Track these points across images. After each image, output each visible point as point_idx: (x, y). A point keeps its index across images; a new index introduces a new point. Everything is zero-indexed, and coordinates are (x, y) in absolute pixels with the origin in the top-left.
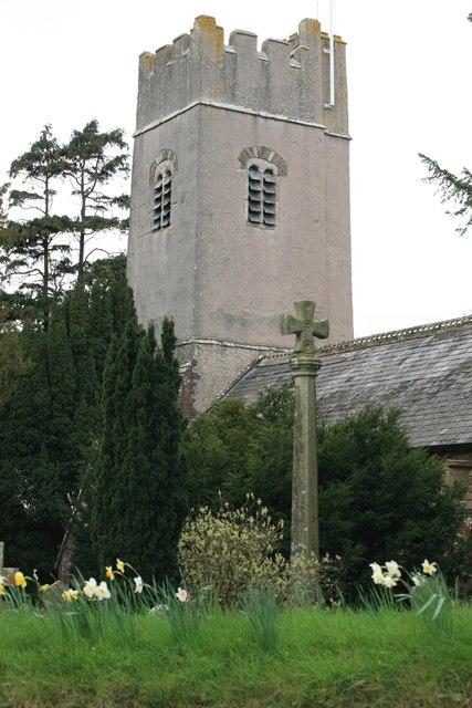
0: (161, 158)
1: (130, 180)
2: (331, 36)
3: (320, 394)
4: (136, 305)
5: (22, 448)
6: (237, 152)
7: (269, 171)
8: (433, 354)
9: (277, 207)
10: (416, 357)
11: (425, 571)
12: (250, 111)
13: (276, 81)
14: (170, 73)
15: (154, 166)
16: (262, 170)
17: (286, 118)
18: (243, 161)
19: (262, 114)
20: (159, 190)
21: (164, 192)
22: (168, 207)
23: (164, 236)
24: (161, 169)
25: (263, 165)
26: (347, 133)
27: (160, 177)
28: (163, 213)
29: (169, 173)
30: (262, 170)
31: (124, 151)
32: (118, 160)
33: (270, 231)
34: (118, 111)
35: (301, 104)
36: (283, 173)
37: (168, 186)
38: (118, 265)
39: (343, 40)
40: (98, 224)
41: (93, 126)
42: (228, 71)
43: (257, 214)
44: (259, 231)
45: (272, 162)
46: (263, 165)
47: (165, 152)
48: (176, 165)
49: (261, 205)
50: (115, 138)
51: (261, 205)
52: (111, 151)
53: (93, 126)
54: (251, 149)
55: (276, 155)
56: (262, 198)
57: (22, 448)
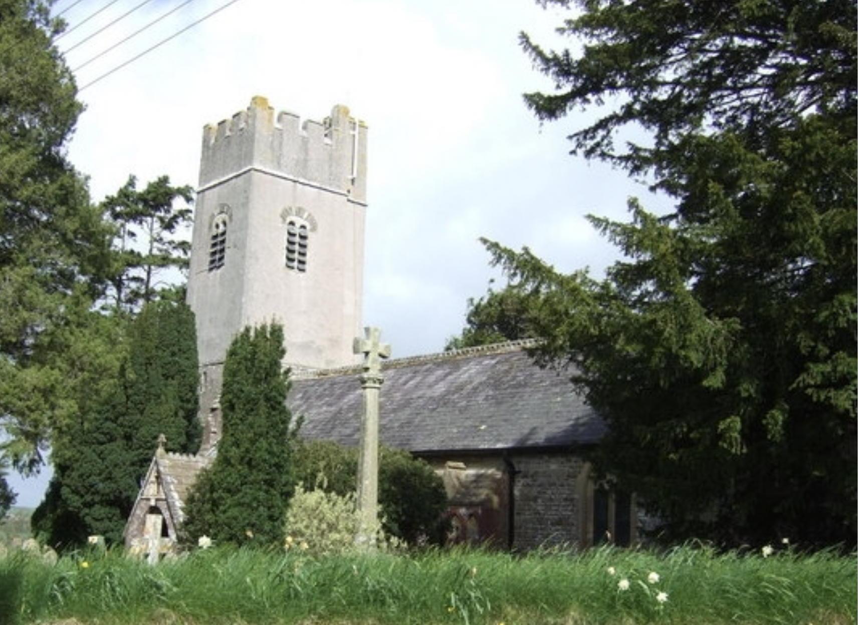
0: (218, 211)
1: (191, 229)
2: (357, 121)
3: (567, 88)
4: (197, 327)
5: (102, 438)
6: (280, 211)
7: (303, 227)
8: (432, 378)
9: (309, 247)
10: (418, 379)
11: (97, 506)
12: (291, 177)
13: (312, 155)
14: (229, 143)
15: (213, 217)
16: (298, 225)
17: (318, 185)
18: (284, 217)
19: (302, 180)
20: (215, 237)
21: (220, 239)
22: (222, 250)
23: (218, 276)
24: (219, 219)
25: (299, 222)
26: (365, 200)
27: (217, 226)
28: (217, 256)
29: (225, 223)
30: (298, 225)
31: (191, 207)
32: (183, 213)
33: (301, 275)
34: (184, 172)
35: (331, 174)
36: (314, 229)
37: (223, 234)
38: (182, 293)
39: (366, 124)
40: (165, 261)
41: (165, 180)
42: (276, 143)
43: (292, 260)
44: (294, 273)
45: (306, 219)
46: (299, 222)
47: (222, 206)
48: (231, 217)
49: (296, 252)
50: (185, 192)
51: (296, 252)
52: (178, 204)
53: (165, 180)
54: (291, 209)
55: (309, 215)
56: (297, 247)
57: (102, 438)
